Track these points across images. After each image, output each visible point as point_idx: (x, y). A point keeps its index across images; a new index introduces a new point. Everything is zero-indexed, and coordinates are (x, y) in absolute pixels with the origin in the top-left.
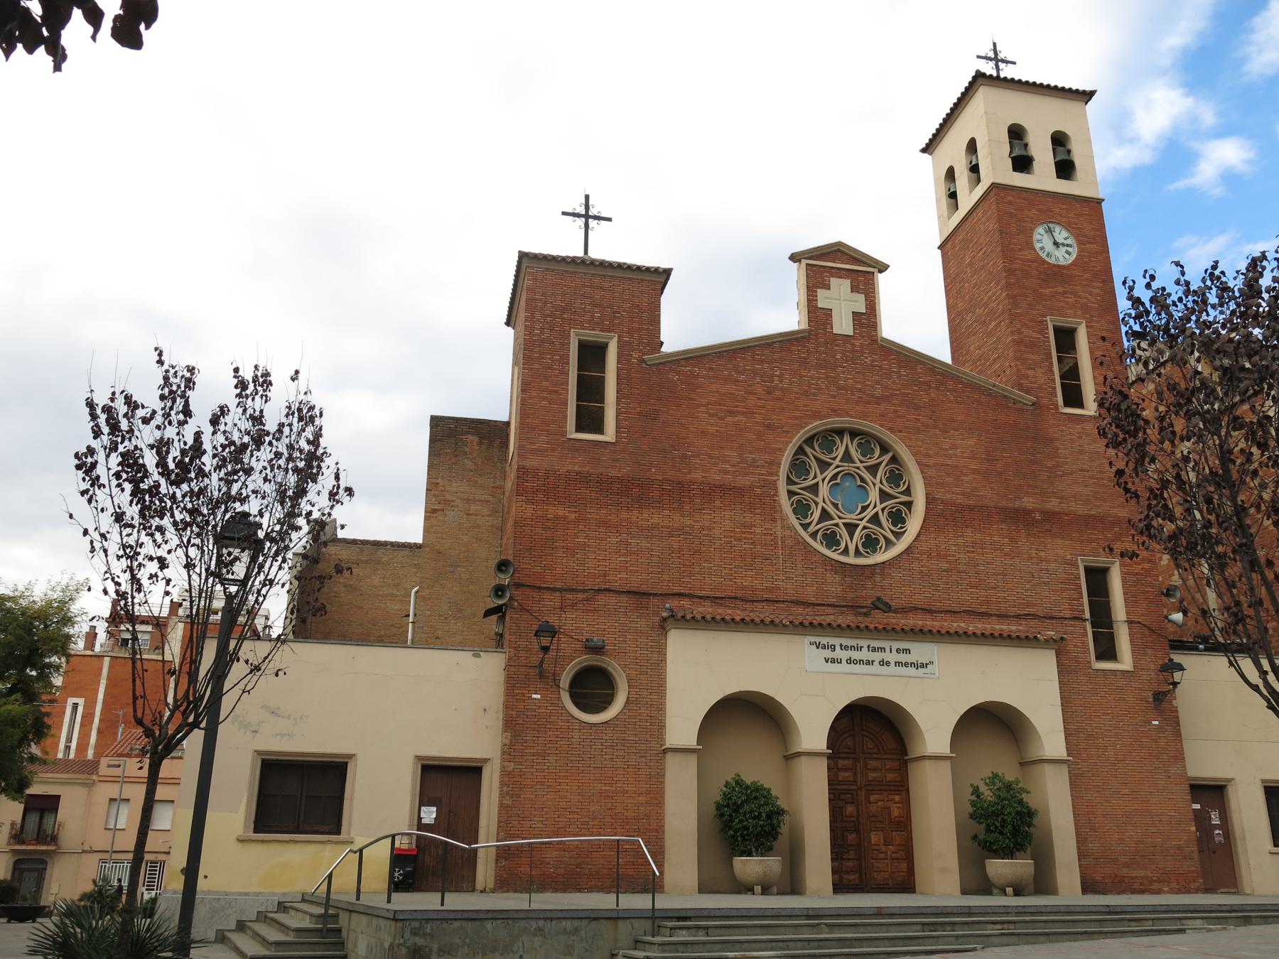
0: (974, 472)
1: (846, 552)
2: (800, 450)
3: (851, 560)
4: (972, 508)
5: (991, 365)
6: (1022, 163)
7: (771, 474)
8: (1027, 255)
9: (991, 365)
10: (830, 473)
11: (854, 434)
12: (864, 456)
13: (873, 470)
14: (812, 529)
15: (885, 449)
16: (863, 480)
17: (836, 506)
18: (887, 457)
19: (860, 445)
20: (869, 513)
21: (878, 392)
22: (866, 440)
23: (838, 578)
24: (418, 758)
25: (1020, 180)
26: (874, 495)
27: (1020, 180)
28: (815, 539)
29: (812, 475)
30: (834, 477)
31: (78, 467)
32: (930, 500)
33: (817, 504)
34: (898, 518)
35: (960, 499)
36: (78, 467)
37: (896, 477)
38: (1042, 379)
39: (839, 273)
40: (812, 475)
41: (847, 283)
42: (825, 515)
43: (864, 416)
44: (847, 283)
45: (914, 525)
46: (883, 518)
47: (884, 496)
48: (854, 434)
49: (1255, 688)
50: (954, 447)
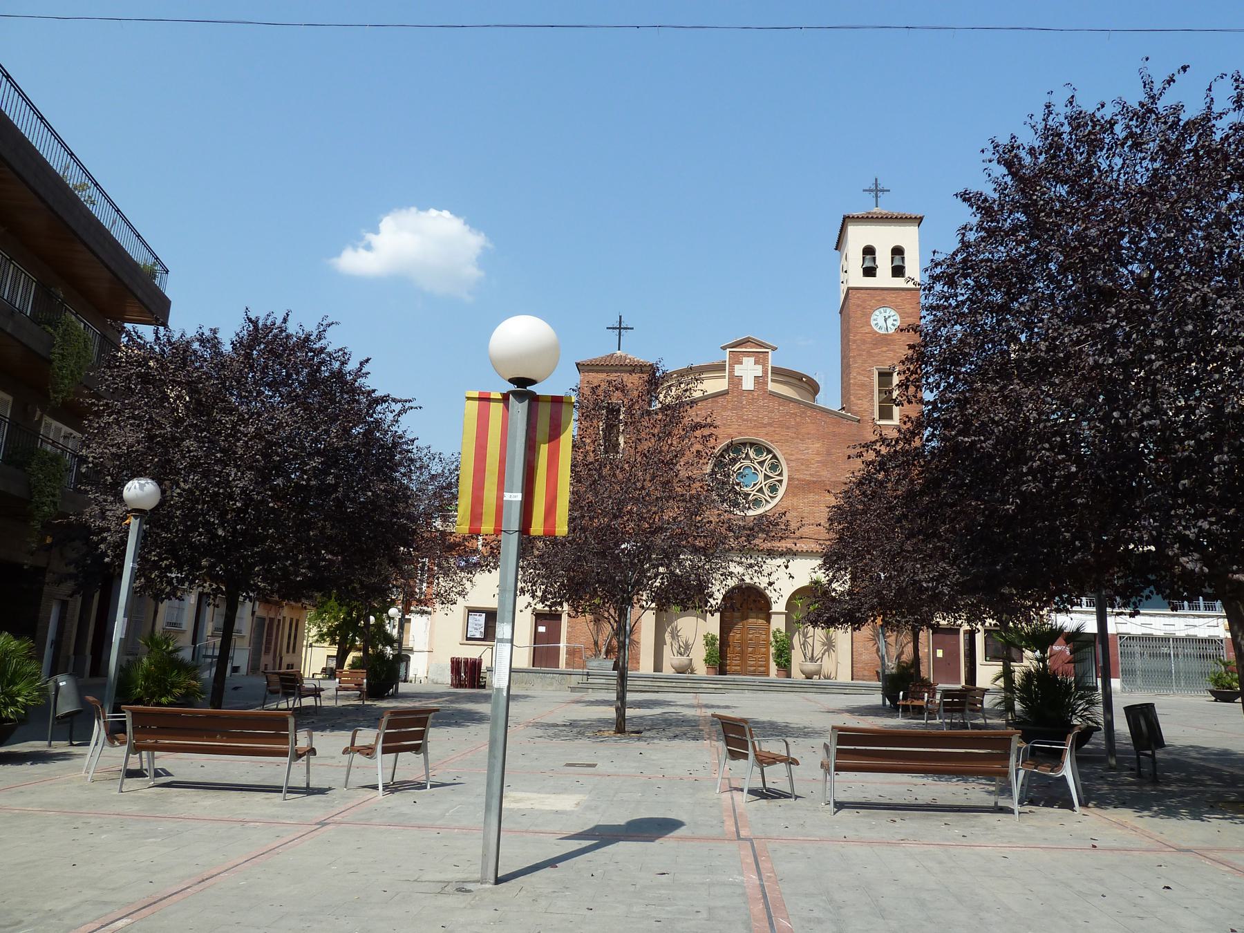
0: (818, 462)
1: (780, 481)
3: (785, 478)
4: (814, 482)
5: (1195, 793)
6: (870, 272)
7: (169, 631)
8: (866, 330)
9: (1195, 793)
11: (752, 445)
13: (761, 463)
15: (769, 452)
21: (766, 421)
22: (760, 448)
23: (1142, 180)
25: (869, 282)
26: (761, 477)
27: (869, 282)
32: (790, 479)
34: (773, 489)
35: (808, 478)
37: (774, 467)
38: (866, 405)
39: (748, 354)
41: (752, 359)
43: (757, 435)
44: (752, 359)
45: (782, 491)
46: (765, 490)
47: (767, 477)
48: (752, 445)
49: (1208, 850)
50: (807, 448)
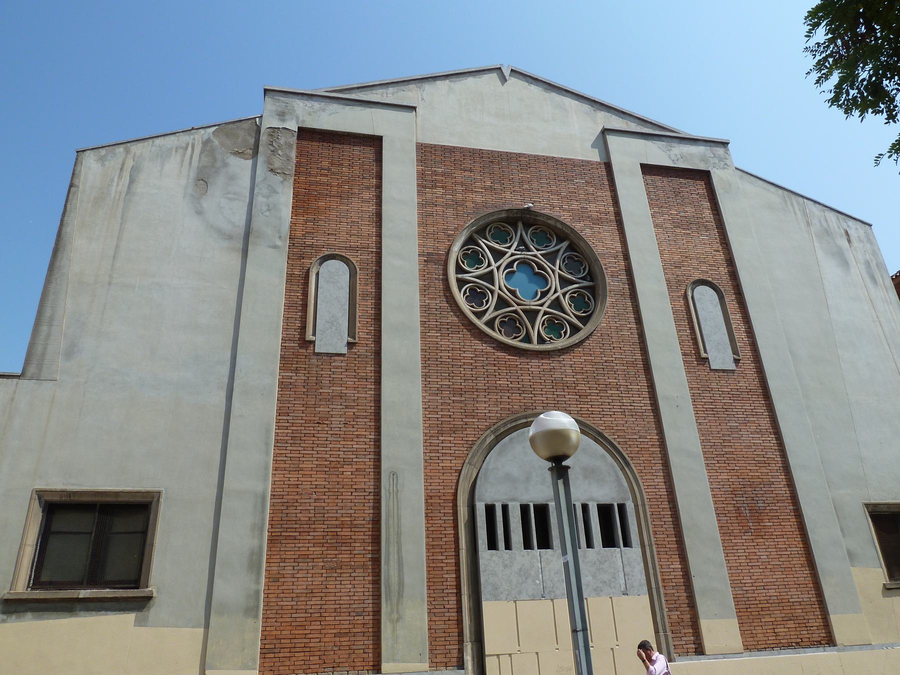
1: (528, 339)
2: (470, 240)
10: (505, 261)
12: (506, 242)
14: (487, 317)
16: (540, 267)
17: (513, 293)
18: (565, 244)
19: (533, 234)
20: (551, 297)
24: (40, 494)
26: (554, 282)
28: (493, 329)
29: (563, 267)
30: (510, 265)
31: (848, 111)
33: (492, 292)
36: (848, 111)
40: (563, 267)
42: (502, 303)
